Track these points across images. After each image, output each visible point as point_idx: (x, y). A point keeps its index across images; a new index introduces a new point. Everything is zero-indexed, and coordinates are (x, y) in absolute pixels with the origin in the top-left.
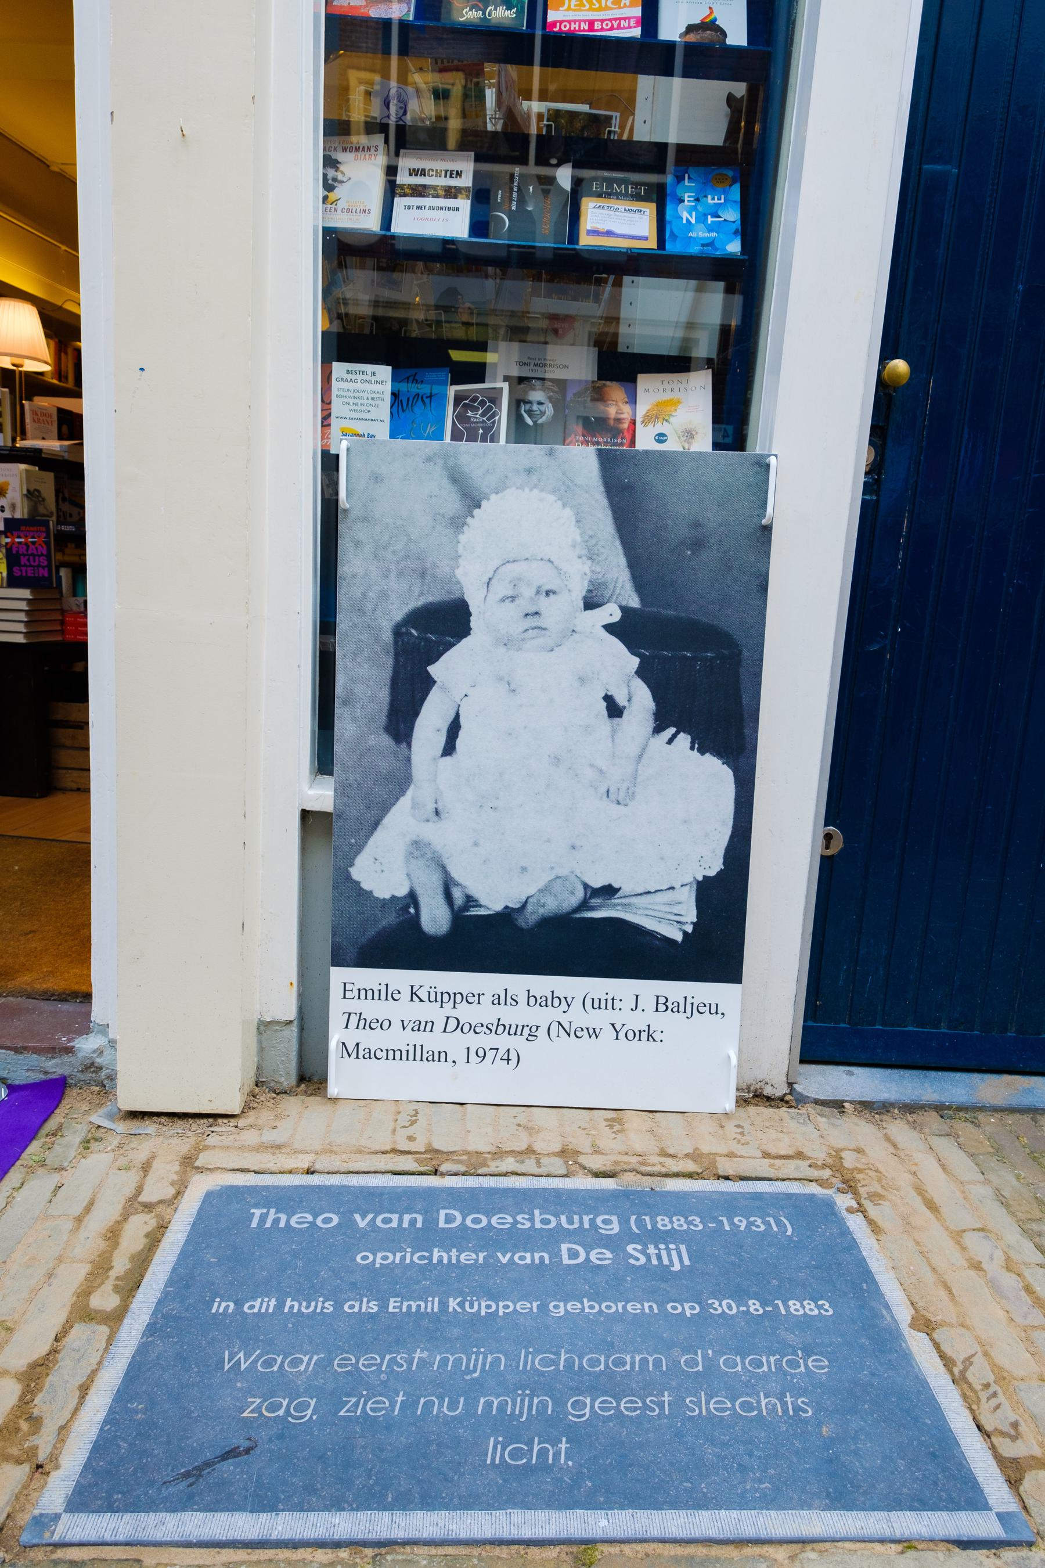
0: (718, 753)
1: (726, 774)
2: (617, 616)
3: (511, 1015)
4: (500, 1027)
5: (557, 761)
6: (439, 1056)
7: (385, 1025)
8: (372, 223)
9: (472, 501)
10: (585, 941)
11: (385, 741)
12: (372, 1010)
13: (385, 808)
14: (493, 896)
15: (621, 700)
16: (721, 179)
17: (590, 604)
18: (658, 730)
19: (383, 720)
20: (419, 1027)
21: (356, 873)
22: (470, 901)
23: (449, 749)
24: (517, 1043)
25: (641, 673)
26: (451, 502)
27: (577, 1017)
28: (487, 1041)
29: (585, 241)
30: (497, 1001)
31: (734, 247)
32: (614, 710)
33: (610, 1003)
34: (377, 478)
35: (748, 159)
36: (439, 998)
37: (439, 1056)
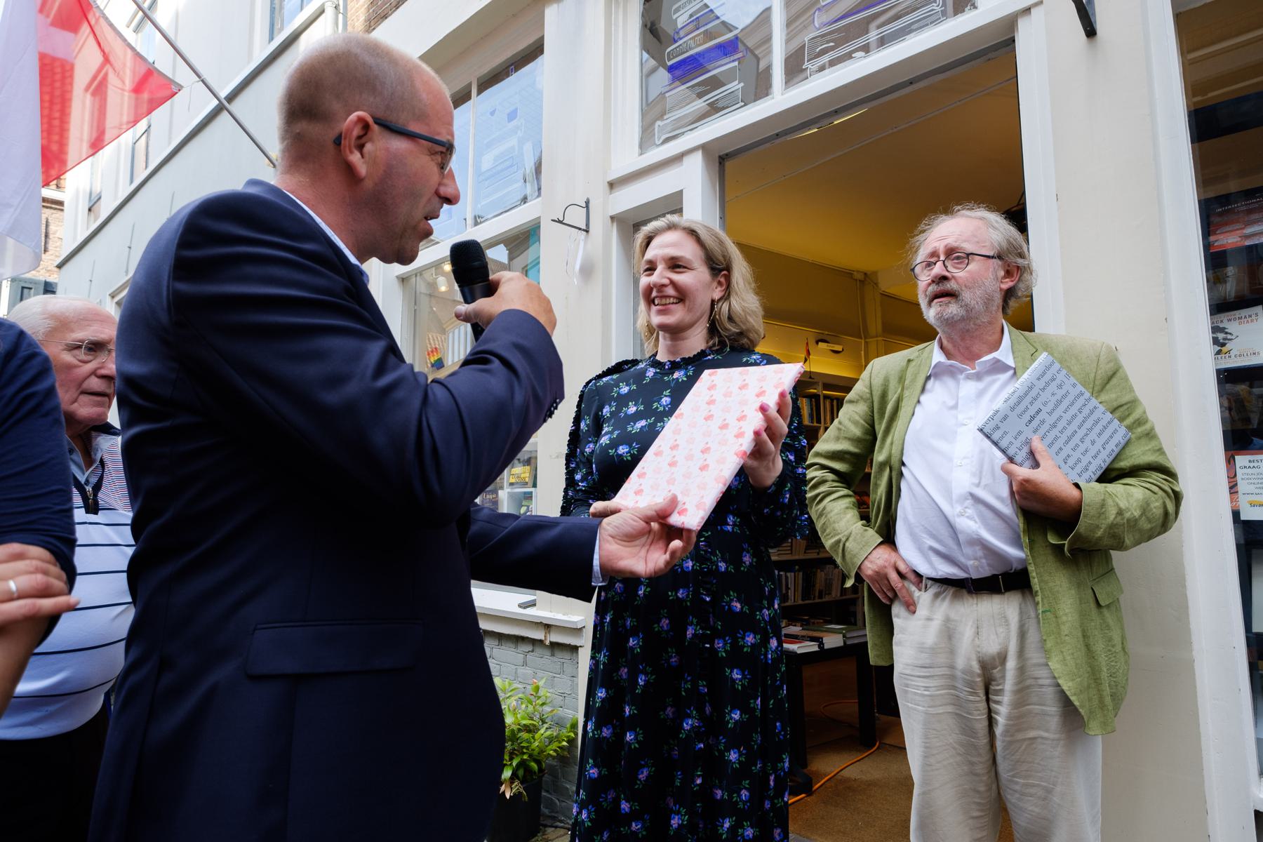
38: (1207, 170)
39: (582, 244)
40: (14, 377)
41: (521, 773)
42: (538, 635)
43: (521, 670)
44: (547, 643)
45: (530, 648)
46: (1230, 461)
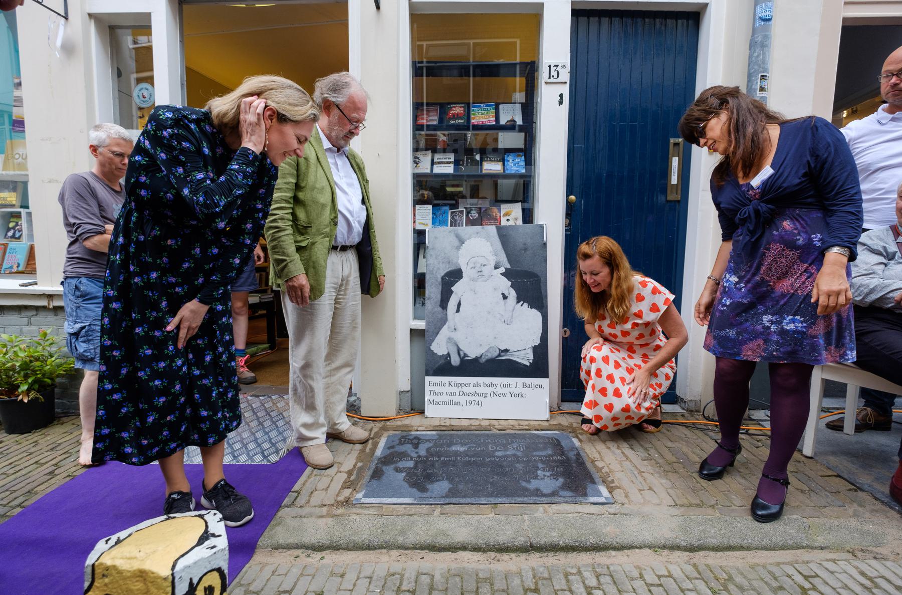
0: (536, 308)
1: (539, 314)
2: (504, 271)
3: (479, 390)
4: (476, 394)
5: (489, 313)
6: (458, 403)
7: (441, 394)
8: (428, 171)
9: (462, 242)
10: (499, 366)
11: (440, 309)
12: (438, 389)
13: (440, 329)
14: (472, 353)
15: (507, 294)
16: (519, 156)
17: (496, 268)
18: (518, 302)
19: (439, 303)
20: (451, 394)
21: (432, 348)
22: (465, 355)
23: (458, 311)
24: (481, 399)
25: (511, 286)
26: (457, 243)
27: (499, 390)
28: (472, 398)
29: (484, 172)
30: (474, 386)
31: (524, 171)
32: (505, 297)
33: (509, 385)
34: (436, 238)
35: (528, 152)
36: (457, 385)
37: (458, 403)
38: (417, 90)
39: (62, 29)
40: (836, 186)
41: (36, 386)
42: (44, 303)
43: (25, 329)
44: (51, 307)
45: (34, 313)
46: (414, 206)
